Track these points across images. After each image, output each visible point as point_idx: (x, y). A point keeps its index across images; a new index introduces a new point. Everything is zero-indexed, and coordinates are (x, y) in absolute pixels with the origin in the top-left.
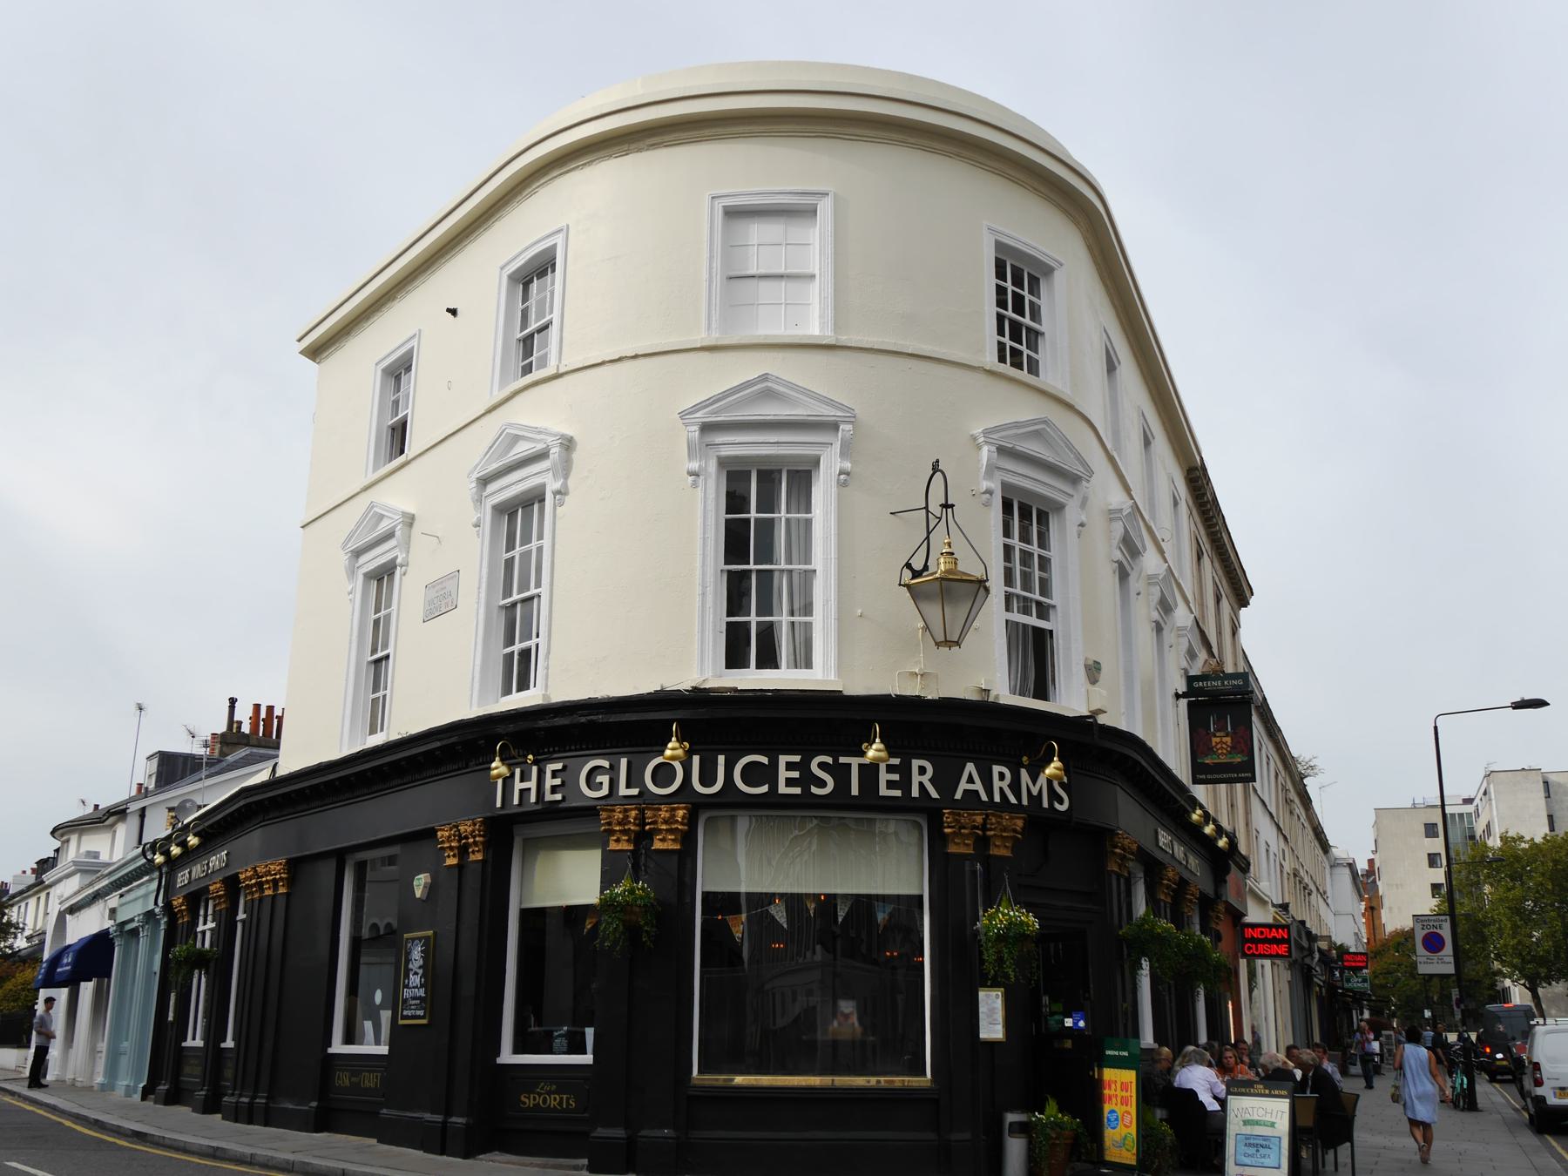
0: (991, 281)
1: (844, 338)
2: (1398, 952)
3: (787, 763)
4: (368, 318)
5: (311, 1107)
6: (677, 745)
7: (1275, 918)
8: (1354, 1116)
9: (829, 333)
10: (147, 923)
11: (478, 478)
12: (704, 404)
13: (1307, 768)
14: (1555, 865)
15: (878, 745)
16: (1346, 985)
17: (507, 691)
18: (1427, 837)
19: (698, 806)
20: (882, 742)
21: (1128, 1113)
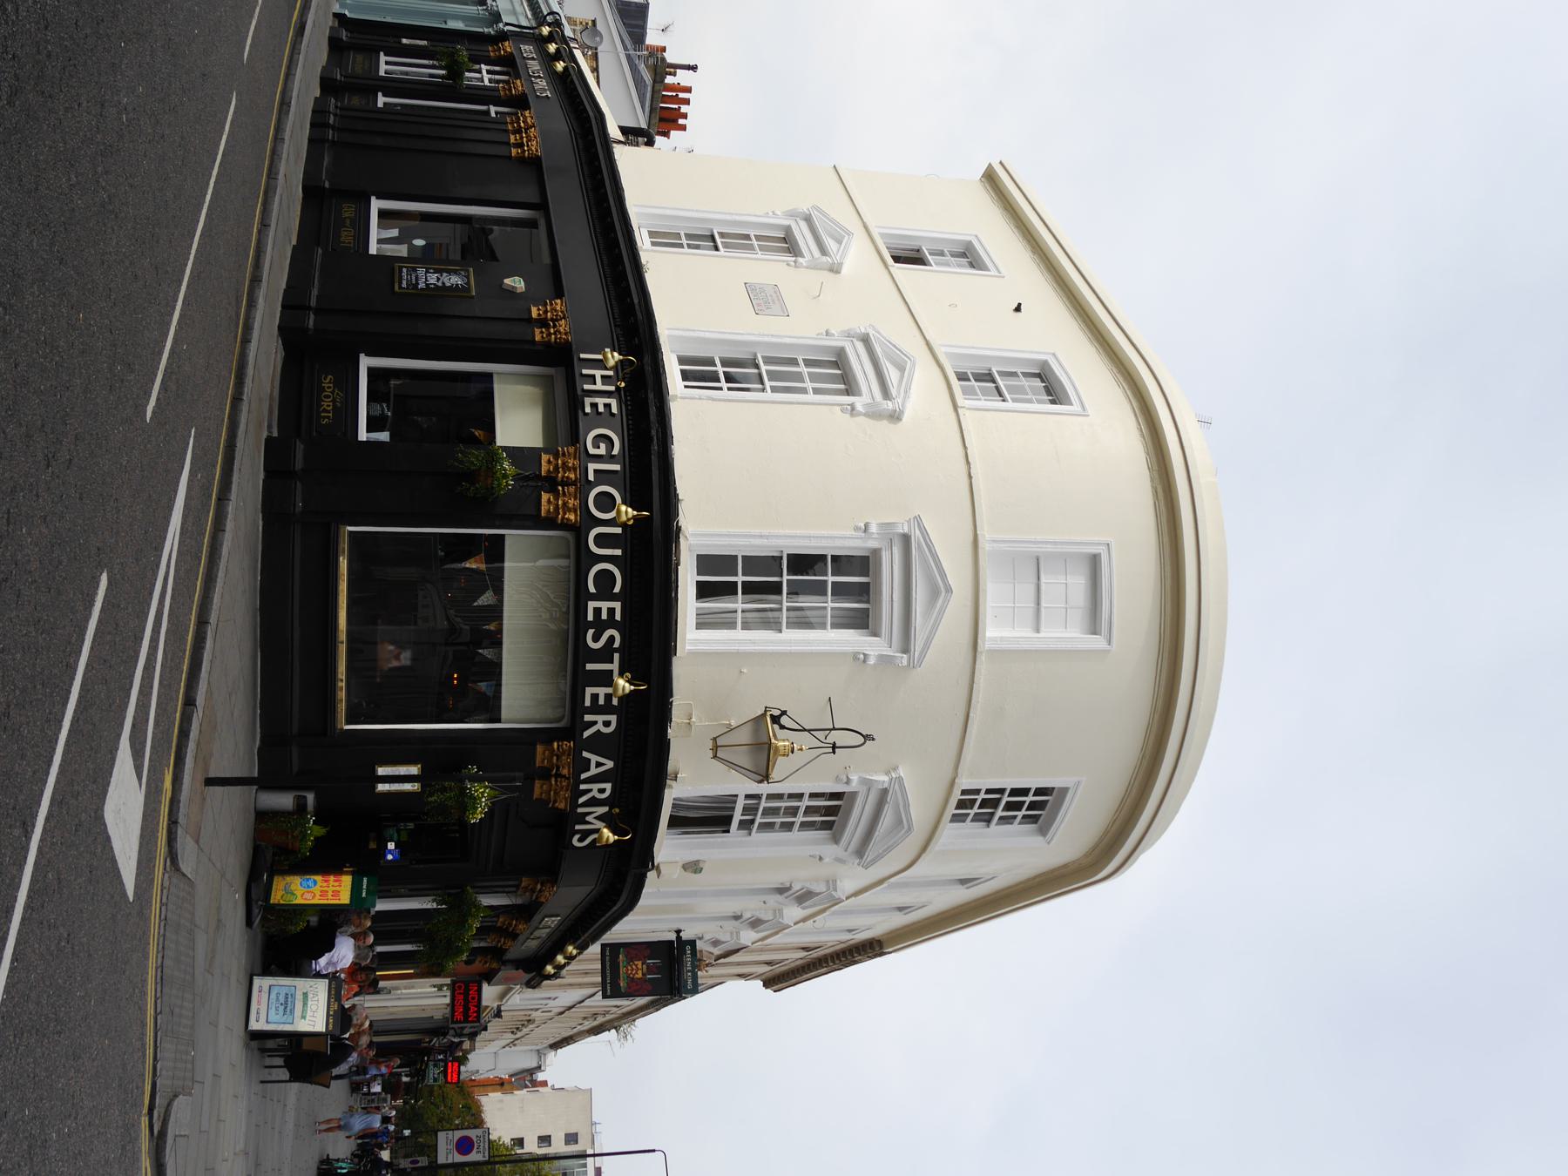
0: (1033, 783)
1: (984, 659)
4: (1018, 227)
6: (630, 516)
8: (311, 1083)
11: (868, 334)
15: (628, 688)
16: (431, 1063)
18: (566, 1135)
19: (578, 532)
20: (631, 691)
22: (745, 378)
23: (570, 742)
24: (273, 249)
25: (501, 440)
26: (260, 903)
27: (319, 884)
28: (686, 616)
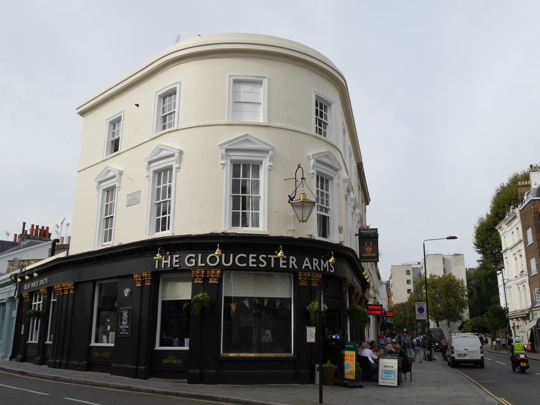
0: (314, 107)
5: (84, 363)
6: (219, 251)
7: (374, 303)
9: (266, 122)
10: (10, 301)
11: (148, 161)
12: (227, 143)
14: (446, 284)
15: (281, 252)
16: (386, 322)
17: (158, 230)
18: (407, 275)
19: (224, 269)
20: (282, 251)
21: (353, 364)
22: (165, 207)
24: (115, 382)
25: (189, 298)
26: (355, 383)
27: (348, 362)
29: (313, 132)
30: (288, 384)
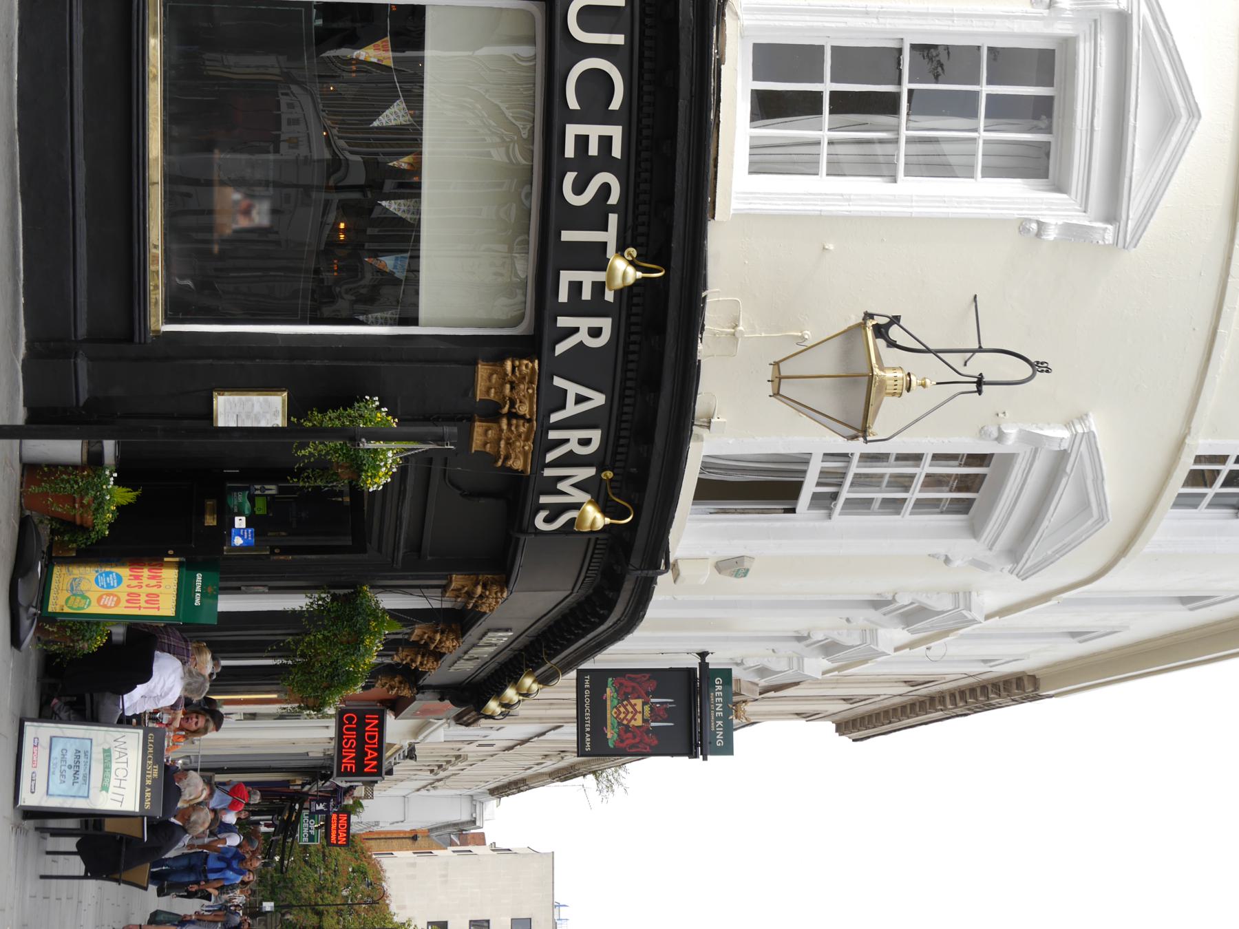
2: (353, 871)
3: (611, 138)
7: (392, 745)
8: (118, 881)
13: (609, 781)
15: (633, 275)
16: (305, 812)
18: (512, 919)
21: (118, 602)
23: (532, 362)
26: (32, 610)
27: (125, 582)
28: (732, 153)
29: (1201, 441)
30: (24, 305)
